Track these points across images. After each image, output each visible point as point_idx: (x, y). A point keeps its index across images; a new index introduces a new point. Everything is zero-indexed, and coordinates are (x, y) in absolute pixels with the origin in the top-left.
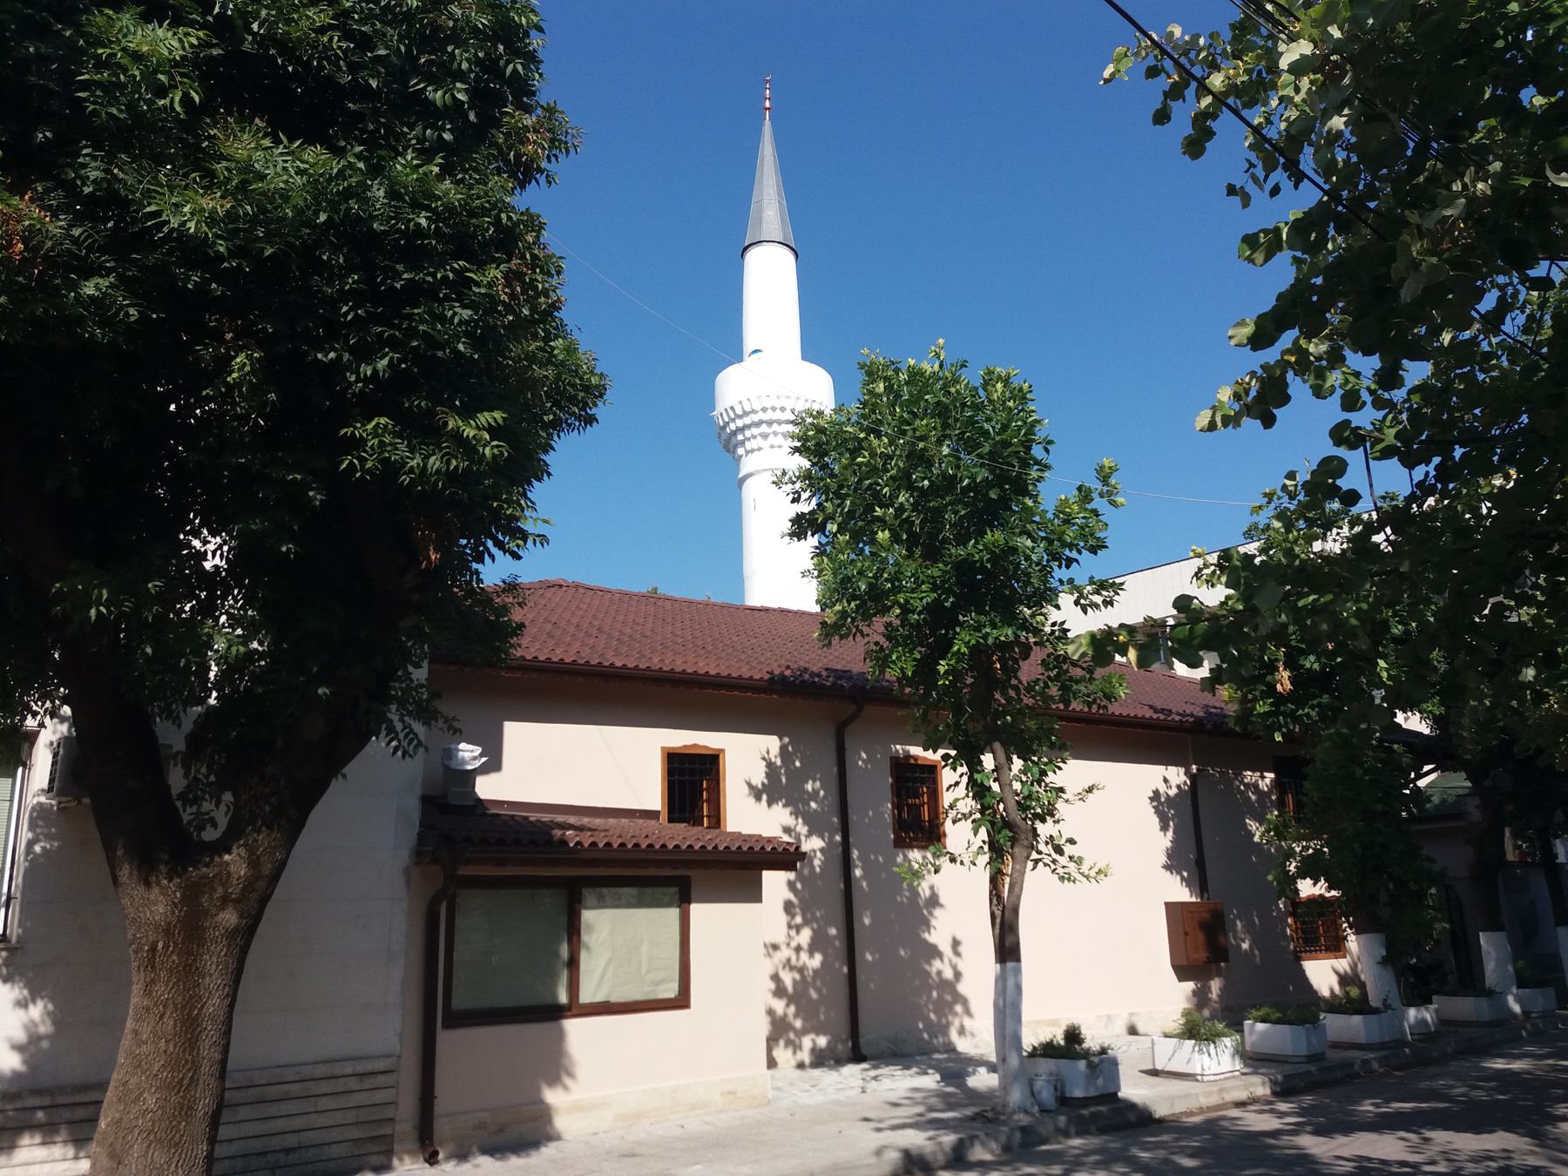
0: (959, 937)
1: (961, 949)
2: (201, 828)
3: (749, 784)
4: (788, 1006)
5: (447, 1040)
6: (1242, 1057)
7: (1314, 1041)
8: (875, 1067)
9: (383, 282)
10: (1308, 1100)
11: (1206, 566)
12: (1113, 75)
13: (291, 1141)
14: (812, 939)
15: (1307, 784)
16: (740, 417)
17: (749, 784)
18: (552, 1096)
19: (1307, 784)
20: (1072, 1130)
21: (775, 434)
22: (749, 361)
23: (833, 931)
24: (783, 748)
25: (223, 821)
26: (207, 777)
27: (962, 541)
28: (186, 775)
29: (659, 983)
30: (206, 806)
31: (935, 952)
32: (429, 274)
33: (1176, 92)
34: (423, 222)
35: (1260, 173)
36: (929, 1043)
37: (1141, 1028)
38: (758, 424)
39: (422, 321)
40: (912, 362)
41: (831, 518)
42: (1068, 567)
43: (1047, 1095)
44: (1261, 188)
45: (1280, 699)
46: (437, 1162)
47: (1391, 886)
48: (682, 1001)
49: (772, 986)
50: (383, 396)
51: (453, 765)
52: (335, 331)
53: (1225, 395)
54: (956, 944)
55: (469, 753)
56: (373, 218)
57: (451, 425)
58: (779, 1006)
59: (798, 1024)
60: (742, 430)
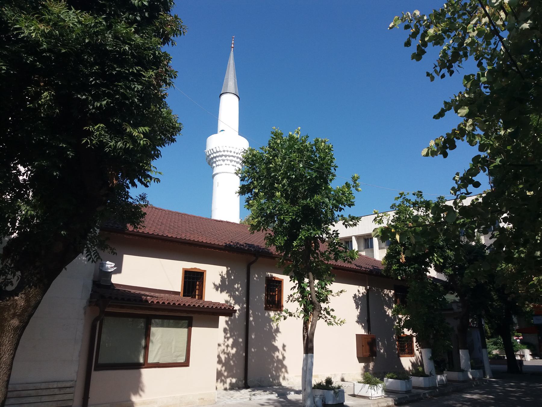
0: (285, 344)
1: (286, 348)
2: (6, 285)
3: (214, 284)
4: (222, 367)
5: (96, 375)
6: (385, 391)
7: (408, 386)
8: (253, 391)
9: (108, 71)
11: (378, 217)
12: (393, 26)
14: (233, 342)
15: (408, 295)
16: (215, 153)
17: (214, 284)
19: (408, 295)
21: (227, 160)
22: (219, 134)
23: (241, 340)
24: (228, 271)
26: (11, 265)
27: (305, 198)
29: (178, 357)
30: (9, 277)
31: (276, 349)
32: (127, 70)
33: (414, 35)
34: (127, 48)
35: (438, 69)
36: (272, 382)
38: (221, 156)
39: (122, 88)
40: (291, 133)
41: (255, 187)
42: (340, 211)
44: (438, 75)
45: (401, 265)
48: (186, 364)
49: (217, 359)
50: (102, 116)
51: (104, 270)
52: (85, 88)
53: (432, 143)
54: (284, 346)
55: (110, 265)
56: (107, 45)
57: (128, 130)
58: (219, 367)
60: (215, 157)
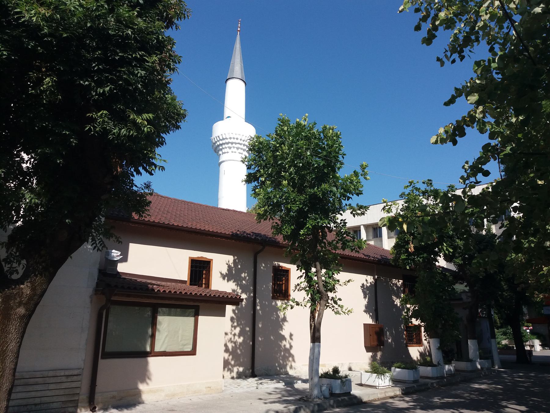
0: (292, 333)
1: (293, 337)
2: (12, 274)
3: (221, 273)
4: (229, 356)
8: (261, 379)
9: (110, 56)
10: (415, 397)
12: (403, 9)
13: (37, 401)
14: (240, 331)
15: (417, 285)
16: (221, 140)
17: (221, 273)
18: (142, 387)
19: (417, 285)
20: (335, 406)
21: (234, 147)
22: (226, 121)
23: (248, 329)
24: (234, 260)
25: (21, 272)
26: (16, 253)
27: (312, 187)
28: (7, 252)
30: (14, 265)
31: (283, 338)
34: (130, 33)
35: (449, 54)
36: (279, 371)
37: (353, 368)
38: (228, 143)
39: (125, 74)
40: (298, 120)
41: (261, 176)
42: (348, 200)
43: (327, 394)
44: (448, 60)
45: (410, 254)
46: (95, 411)
47: (443, 322)
48: (193, 352)
49: (224, 348)
50: (105, 102)
51: (109, 258)
52: (87, 73)
53: (442, 130)
54: (291, 335)
55: (116, 254)
56: (109, 29)
57: (132, 117)
58: (226, 355)
59: (233, 363)
